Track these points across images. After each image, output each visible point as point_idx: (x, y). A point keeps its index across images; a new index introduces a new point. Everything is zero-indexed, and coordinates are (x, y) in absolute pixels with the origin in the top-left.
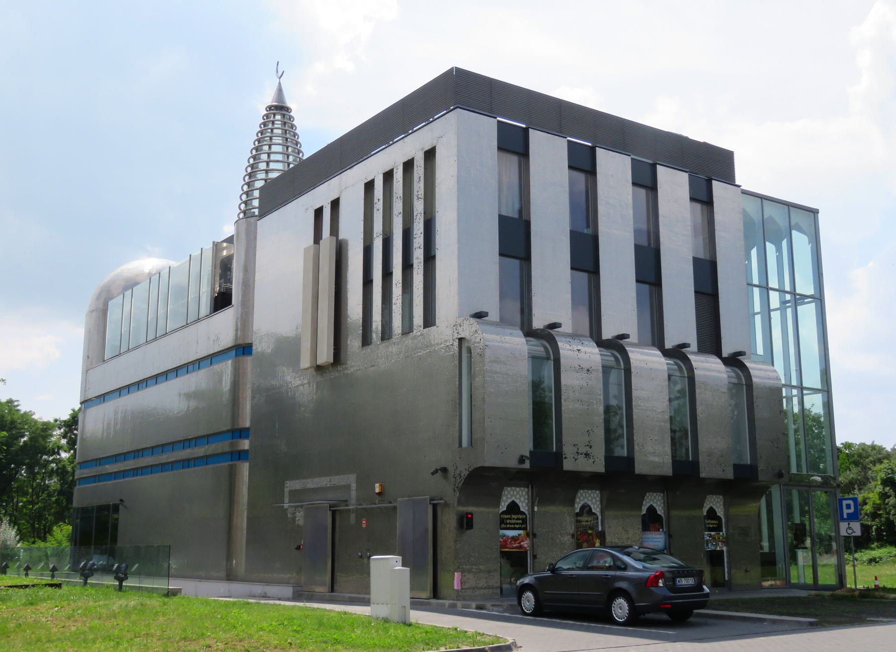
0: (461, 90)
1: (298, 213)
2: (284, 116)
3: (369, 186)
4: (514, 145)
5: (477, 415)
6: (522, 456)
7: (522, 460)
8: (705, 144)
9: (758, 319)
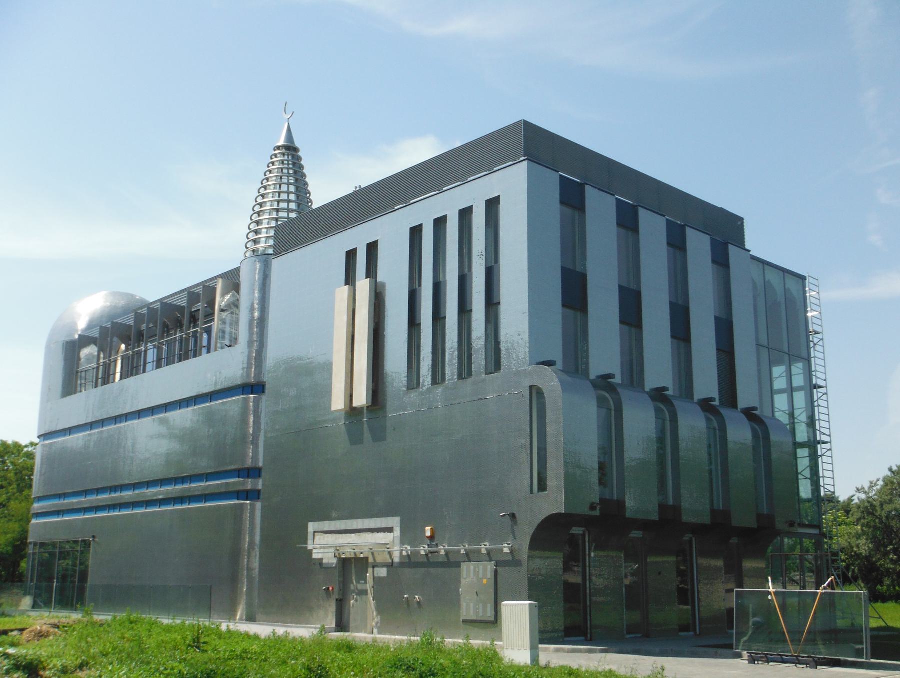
0: (536, 145)
1: (330, 251)
2: (293, 157)
3: (416, 233)
4: (572, 198)
5: (205, 465)
6: (593, 504)
7: (593, 507)
8: (722, 210)
9: (100, 376)
